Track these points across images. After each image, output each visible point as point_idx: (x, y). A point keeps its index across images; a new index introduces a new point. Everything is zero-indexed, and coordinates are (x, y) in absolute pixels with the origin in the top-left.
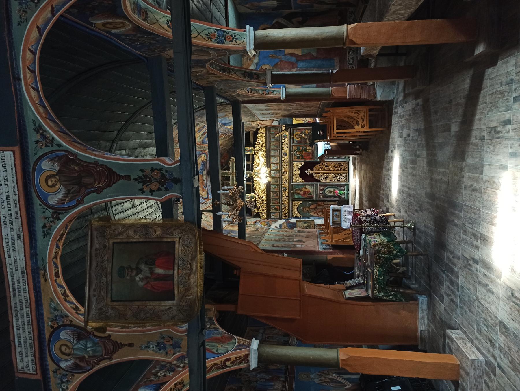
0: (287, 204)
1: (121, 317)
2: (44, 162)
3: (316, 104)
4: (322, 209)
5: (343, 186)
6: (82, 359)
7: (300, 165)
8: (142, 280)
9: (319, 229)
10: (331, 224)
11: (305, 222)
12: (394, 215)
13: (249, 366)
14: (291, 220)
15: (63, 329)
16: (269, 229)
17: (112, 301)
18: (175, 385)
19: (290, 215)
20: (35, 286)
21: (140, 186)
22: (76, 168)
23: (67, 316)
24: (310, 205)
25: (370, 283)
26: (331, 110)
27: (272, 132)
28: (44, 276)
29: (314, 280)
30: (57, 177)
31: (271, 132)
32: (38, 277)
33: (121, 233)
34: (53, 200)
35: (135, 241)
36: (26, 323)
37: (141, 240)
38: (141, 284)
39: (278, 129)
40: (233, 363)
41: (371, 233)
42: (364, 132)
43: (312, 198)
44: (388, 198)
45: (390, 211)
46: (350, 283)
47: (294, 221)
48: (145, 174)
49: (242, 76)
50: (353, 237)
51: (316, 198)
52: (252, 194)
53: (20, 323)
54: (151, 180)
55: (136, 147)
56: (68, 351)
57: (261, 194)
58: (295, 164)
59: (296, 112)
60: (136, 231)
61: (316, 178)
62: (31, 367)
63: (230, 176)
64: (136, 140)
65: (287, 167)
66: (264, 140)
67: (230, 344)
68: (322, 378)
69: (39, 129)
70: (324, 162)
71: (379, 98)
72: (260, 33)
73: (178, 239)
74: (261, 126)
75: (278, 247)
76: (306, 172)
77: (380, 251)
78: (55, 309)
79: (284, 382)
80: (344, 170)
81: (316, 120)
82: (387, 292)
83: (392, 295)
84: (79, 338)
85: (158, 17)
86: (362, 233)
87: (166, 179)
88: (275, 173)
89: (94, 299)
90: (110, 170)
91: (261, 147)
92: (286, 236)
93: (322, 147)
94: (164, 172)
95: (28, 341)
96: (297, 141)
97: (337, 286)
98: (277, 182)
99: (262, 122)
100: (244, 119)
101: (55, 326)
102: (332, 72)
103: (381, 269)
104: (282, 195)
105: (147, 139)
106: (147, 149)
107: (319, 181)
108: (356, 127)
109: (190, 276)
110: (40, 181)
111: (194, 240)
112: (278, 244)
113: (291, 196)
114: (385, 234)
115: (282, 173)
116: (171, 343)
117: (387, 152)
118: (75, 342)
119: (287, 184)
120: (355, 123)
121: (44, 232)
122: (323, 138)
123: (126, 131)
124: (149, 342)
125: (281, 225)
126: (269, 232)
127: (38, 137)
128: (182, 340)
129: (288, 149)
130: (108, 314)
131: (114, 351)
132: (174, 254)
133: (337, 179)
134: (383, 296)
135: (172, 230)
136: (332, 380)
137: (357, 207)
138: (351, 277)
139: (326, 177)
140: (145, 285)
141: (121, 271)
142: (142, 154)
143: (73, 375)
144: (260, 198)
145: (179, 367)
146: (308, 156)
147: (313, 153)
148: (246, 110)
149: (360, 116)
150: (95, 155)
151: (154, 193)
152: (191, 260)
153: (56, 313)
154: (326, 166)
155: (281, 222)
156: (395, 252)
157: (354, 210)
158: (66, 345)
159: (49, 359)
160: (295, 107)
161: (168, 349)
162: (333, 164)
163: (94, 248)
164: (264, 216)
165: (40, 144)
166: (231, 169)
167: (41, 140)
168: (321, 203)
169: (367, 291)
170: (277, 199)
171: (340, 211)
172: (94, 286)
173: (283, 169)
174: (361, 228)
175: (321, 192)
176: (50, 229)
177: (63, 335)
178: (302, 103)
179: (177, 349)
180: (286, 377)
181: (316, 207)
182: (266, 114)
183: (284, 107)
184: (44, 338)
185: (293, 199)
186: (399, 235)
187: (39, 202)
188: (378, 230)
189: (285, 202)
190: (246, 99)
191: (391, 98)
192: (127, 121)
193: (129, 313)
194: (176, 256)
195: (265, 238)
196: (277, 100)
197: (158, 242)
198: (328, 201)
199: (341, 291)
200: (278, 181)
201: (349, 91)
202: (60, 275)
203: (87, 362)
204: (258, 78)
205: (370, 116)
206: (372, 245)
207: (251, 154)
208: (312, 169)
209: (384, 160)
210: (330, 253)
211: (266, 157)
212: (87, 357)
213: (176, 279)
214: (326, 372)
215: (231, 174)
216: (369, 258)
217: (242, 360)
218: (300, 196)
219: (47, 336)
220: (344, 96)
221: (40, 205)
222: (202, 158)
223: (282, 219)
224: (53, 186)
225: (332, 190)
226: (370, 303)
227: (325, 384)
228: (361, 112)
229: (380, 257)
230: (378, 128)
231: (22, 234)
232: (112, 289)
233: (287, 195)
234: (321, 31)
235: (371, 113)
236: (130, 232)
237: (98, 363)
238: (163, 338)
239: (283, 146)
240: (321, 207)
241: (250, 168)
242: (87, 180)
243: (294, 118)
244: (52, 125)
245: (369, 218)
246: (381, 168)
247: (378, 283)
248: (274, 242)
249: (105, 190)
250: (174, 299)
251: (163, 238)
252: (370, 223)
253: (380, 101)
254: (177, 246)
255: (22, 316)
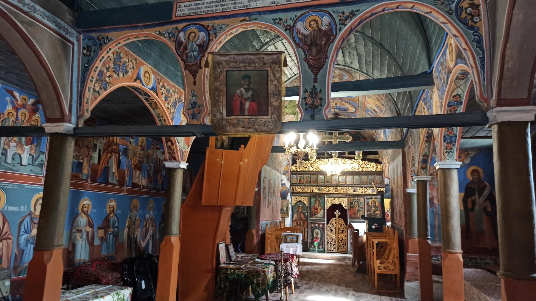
0: (305, 191)
1: (215, 78)
2: (328, 18)
3: (401, 223)
4: (300, 225)
5: (322, 247)
6: (186, 48)
7: (344, 205)
8: (241, 92)
9: (280, 222)
10: (285, 234)
11: (287, 208)
12: (292, 294)
13: (167, 161)
14: (289, 195)
15: (206, 34)
16: (281, 173)
17: (227, 71)
18: (156, 103)
19: (294, 193)
20: (238, 14)
21: (309, 90)
22: (323, 42)
23: (216, 37)
24: (304, 214)
25: (231, 266)
26: (396, 237)
27: (378, 177)
28: (245, 20)
29: (234, 216)
30: (317, 28)
31: (377, 177)
32: (244, 16)
33: (274, 75)
34: (299, 26)
35: (269, 86)
36: (211, 9)
37: (269, 90)
38: (238, 92)
39: (380, 183)
40: (169, 148)
41: (276, 270)
42: (374, 269)
43: (311, 216)
44: (309, 289)
45: (297, 290)
46: (231, 249)
47: (289, 197)
48: (318, 93)
49: (424, 153)
50: (272, 254)
51: (311, 220)
52: (315, 157)
53: (211, 5)
54: (313, 98)
55: (358, 51)
56: (191, 38)
57: (315, 166)
58: (344, 199)
59: (395, 203)
60: (276, 87)
61: (331, 221)
62: (181, 13)
63: (333, 136)
64: (365, 51)
65: (342, 192)
66: (369, 170)
67: (184, 144)
68: (149, 221)
69: (353, 14)
70: (347, 229)
71: (407, 284)
72: (455, 175)
73: (270, 118)
74: (384, 167)
75: (264, 183)
76: (337, 211)
77: (260, 277)
78: (221, 28)
79: (147, 187)
80: (339, 249)
81: (388, 221)
82: (223, 281)
83: (221, 285)
84: (200, 46)
85: (462, 87)
86: (276, 261)
87: (314, 109)
88: (335, 180)
89: (227, 58)
90: (321, 67)
91: (362, 166)
92: (274, 190)
93: (361, 227)
94: (320, 107)
95: (199, 10)
96: (368, 203)
97: (229, 236)
98: (327, 182)
99: (387, 168)
100: (390, 151)
101: (209, 29)
102: (429, 239)
103: (243, 276)
104: (314, 186)
105: (366, 60)
106: (357, 61)
107: (328, 224)
108: (379, 261)
109: (243, 127)
110: (314, 16)
111: (269, 130)
112: (267, 182)
113: (313, 195)
114: (275, 282)
115: (336, 187)
116: (196, 112)
117: (354, 290)
118: (197, 43)
119: (325, 192)
120: (383, 261)
121: (277, 19)
122: (370, 229)
123: (373, 43)
124: (197, 96)
125: (284, 184)
126: (278, 174)
127: (347, 14)
128: (198, 120)
129: (360, 193)
130: (217, 69)
131: (190, 71)
132: (259, 116)
133: (330, 241)
134: (220, 277)
135: (277, 113)
136: (147, 230)
137: (301, 260)
138: (236, 251)
139: (331, 230)
140: (238, 95)
141: (247, 77)
142: (352, 56)
143: (174, 41)
144: (311, 164)
145: (168, 104)
146: (354, 213)
147: (356, 218)
148: (397, 153)
149: (389, 265)
150: (333, 56)
151: (304, 100)
152: (255, 128)
153: (218, 29)
154: (343, 231)
155: (288, 185)
156: (258, 290)
157: (298, 257)
158: (195, 36)
159: (186, 24)
160: (399, 201)
161: (192, 111)
162: (345, 238)
163: (264, 56)
164: (294, 168)
165: (342, 15)
166: (340, 136)
167: (344, 16)
168: (306, 224)
169: (225, 263)
170: (310, 182)
171: (297, 242)
172: (237, 57)
173: (340, 188)
174: (280, 261)
175: (317, 225)
176: (278, 23)
177: (202, 34)
178: (403, 209)
179: (191, 117)
180: (150, 189)
181: (302, 220)
182: (394, 172)
183: (399, 190)
184: (200, 21)
185: (310, 197)
186: (274, 296)
187: (298, 15)
188: (278, 276)
189: (307, 189)
190: (406, 154)
191: (406, 296)
192: (381, 45)
193: (218, 84)
194: (257, 117)
195: (272, 170)
196: (405, 184)
197: (267, 104)
198: (308, 231)
199: (224, 240)
200: (328, 183)
201: (413, 256)
202: (245, 29)
203: (183, 51)
204: (422, 168)
205: (391, 275)
206: (265, 269)
207: (356, 156)
208: (340, 216)
209: (346, 287)
210: (257, 232)
211: (352, 172)
212: (187, 51)
213: (241, 117)
214: (154, 225)
215: (335, 136)
216: (253, 267)
217: (171, 155)
218: (313, 204)
219: (202, 23)
220: (410, 251)
221: (296, 16)
222: (350, 108)
223: (291, 186)
224: (310, 25)
225: (319, 236)
226: (214, 265)
227: (145, 223)
228: (394, 266)
229: (254, 276)
230: (378, 283)
231: (275, 5)
232: (235, 71)
233: (314, 191)
234: (456, 229)
235: (393, 277)
236: (276, 82)
237: (182, 60)
238: (199, 107)
239: (364, 189)
240: (302, 224)
241: (341, 156)
242: (314, 50)
243: (390, 200)
244: (356, 23)
245: (289, 269)
246: (339, 284)
247: (231, 273)
248: (268, 179)
249: (306, 64)
250: (227, 116)
251: (271, 106)
252: (285, 269)
253: (404, 285)
254: (265, 117)
255: (216, 6)
